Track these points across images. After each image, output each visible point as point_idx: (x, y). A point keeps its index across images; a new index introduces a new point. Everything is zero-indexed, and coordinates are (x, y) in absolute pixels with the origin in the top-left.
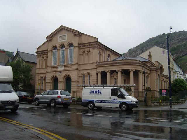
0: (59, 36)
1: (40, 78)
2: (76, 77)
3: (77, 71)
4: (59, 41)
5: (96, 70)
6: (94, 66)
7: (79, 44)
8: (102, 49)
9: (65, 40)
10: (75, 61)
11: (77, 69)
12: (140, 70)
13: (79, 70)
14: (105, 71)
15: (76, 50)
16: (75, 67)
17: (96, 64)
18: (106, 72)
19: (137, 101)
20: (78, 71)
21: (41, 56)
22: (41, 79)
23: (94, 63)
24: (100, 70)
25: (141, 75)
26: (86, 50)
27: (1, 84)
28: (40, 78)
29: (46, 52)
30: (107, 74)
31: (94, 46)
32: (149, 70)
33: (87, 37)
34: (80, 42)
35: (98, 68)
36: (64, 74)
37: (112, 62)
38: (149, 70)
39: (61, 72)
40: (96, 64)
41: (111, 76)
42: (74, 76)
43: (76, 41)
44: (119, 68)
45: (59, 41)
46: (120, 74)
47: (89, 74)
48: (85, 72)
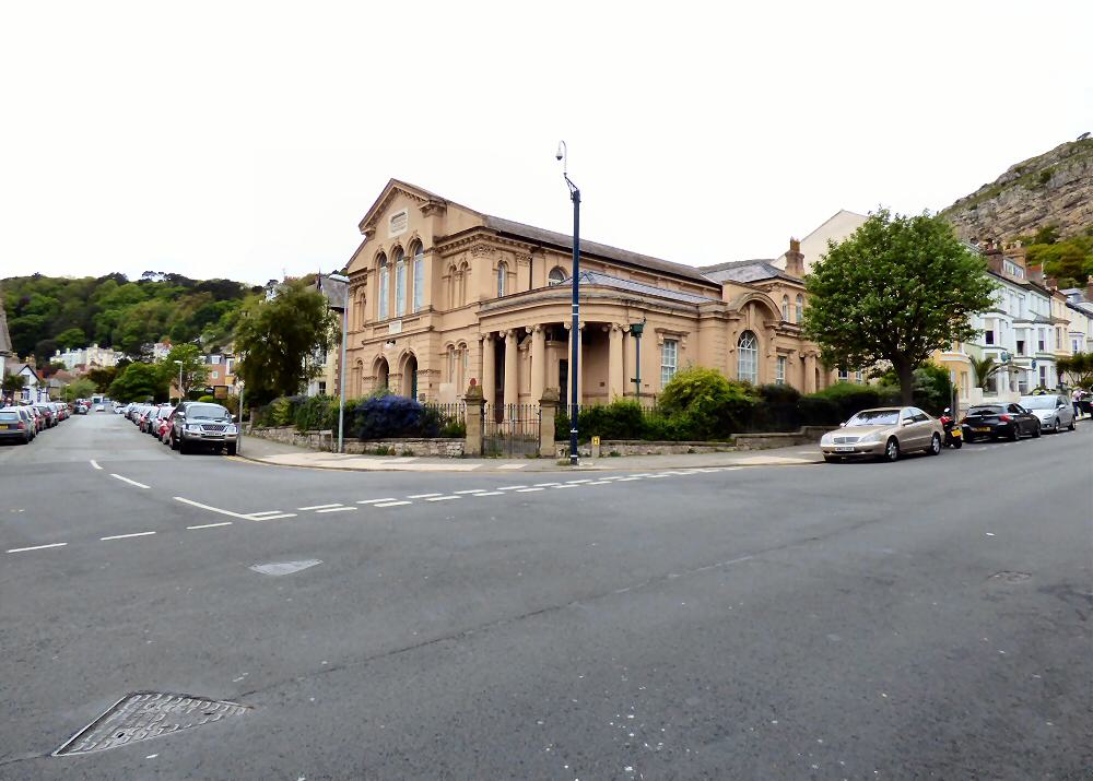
0: (390, 218)
1: (444, 350)
2: (428, 355)
3: (428, 336)
4: (392, 233)
5: (477, 329)
6: (470, 317)
7: (437, 240)
8: (514, 253)
9: (405, 230)
10: (424, 301)
11: (431, 329)
13: (441, 333)
15: (426, 263)
16: (426, 322)
17: (477, 309)
19: (121, 355)
20: (436, 336)
21: (359, 289)
22: (447, 354)
23: (474, 305)
24: (489, 327)
25: (615, 341)
26: (458, 260)
27: (1085, 349)
28: (444, 350)
30: (504, 345)
31: (473, 244)
32: (693, 319)
33: (458, 211)
34: (437, 234)
35: (484, 323)
36: (402, 346)
37: (522, 298)
38: (693, 319)
39: (394, 342)
40: (477, 309)
41: (519, 350)
42: (422, 349)
43: (427, 231)
44: (532, 320)
46: (537, 342)
47: (463, 345)
48: (454, 338)
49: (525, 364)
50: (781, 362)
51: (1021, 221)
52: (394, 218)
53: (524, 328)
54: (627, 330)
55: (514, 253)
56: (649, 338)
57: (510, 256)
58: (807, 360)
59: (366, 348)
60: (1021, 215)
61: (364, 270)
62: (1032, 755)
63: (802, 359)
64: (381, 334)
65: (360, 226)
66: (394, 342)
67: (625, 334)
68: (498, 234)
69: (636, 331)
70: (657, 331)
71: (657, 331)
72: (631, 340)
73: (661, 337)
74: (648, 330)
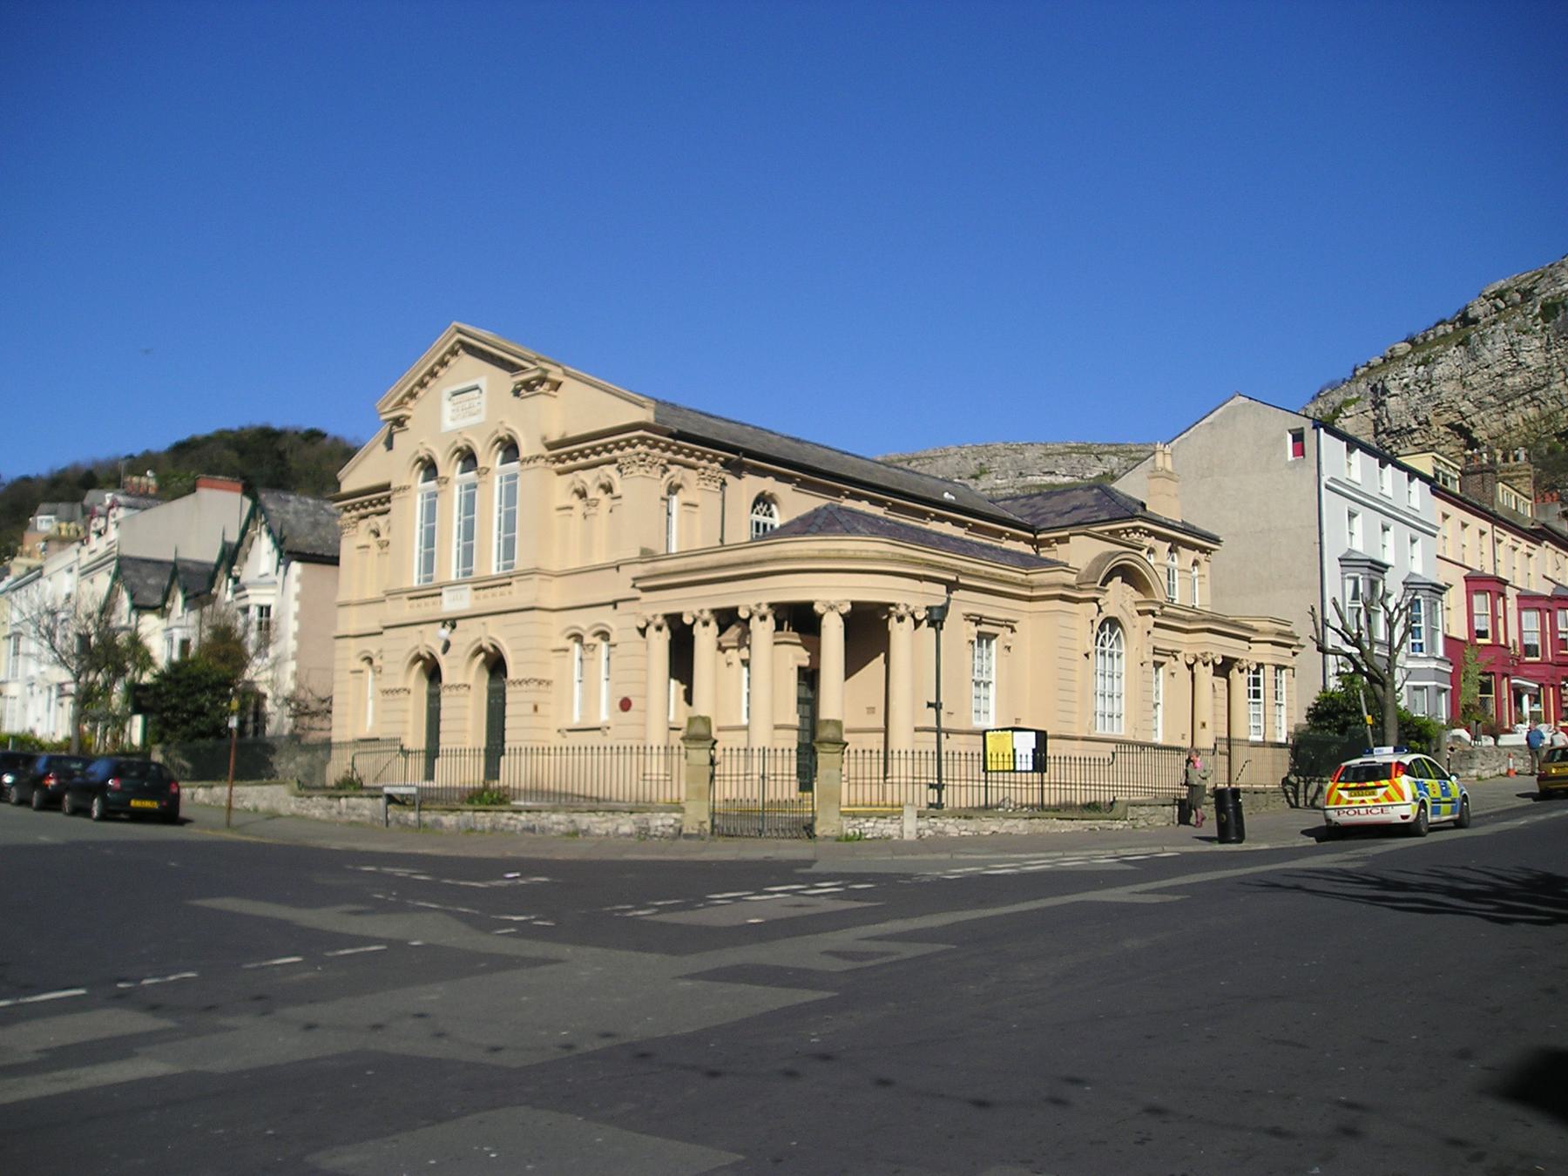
0: (447, 392)
6: (620, 585)
12: (893, 605)
14: (810, 604)
18: (818, 608)
25: (900, 633)
29: (380, 501)
45: (448, 424)
46: (763, 631)
49: (1261, 630)
50: (1157, 670)
51: (1508, 391)
52: (455, 394)
53: (736, 609)
54: (920, 615)
55: (614, 461)
56: (958, 630)
57: (610, 470)
58: (1199, 667)
59: (387, 632)
60: (1508, 381)
61: (386, 487)
62: (1517, 297)
63: (1190, 667)
64: (425, 609)
65: (740, 478)
66: (454, 627)
67: (917, 623)
68: (671, 435)
69: (936, 619)
70: (968, 617)
71: (968, 617)
72: (927, 632)
73: (974, 629)
74: (953, 619)
